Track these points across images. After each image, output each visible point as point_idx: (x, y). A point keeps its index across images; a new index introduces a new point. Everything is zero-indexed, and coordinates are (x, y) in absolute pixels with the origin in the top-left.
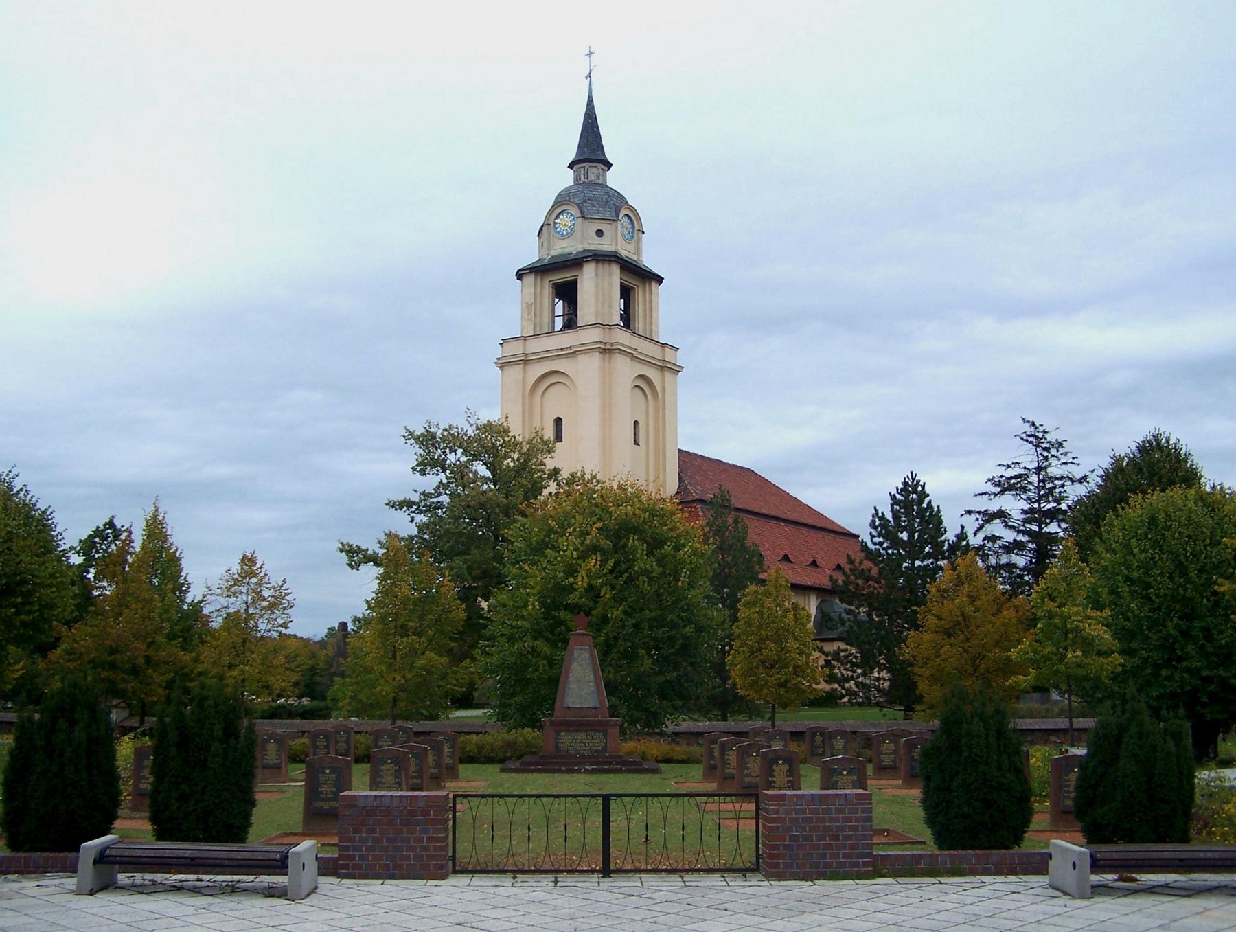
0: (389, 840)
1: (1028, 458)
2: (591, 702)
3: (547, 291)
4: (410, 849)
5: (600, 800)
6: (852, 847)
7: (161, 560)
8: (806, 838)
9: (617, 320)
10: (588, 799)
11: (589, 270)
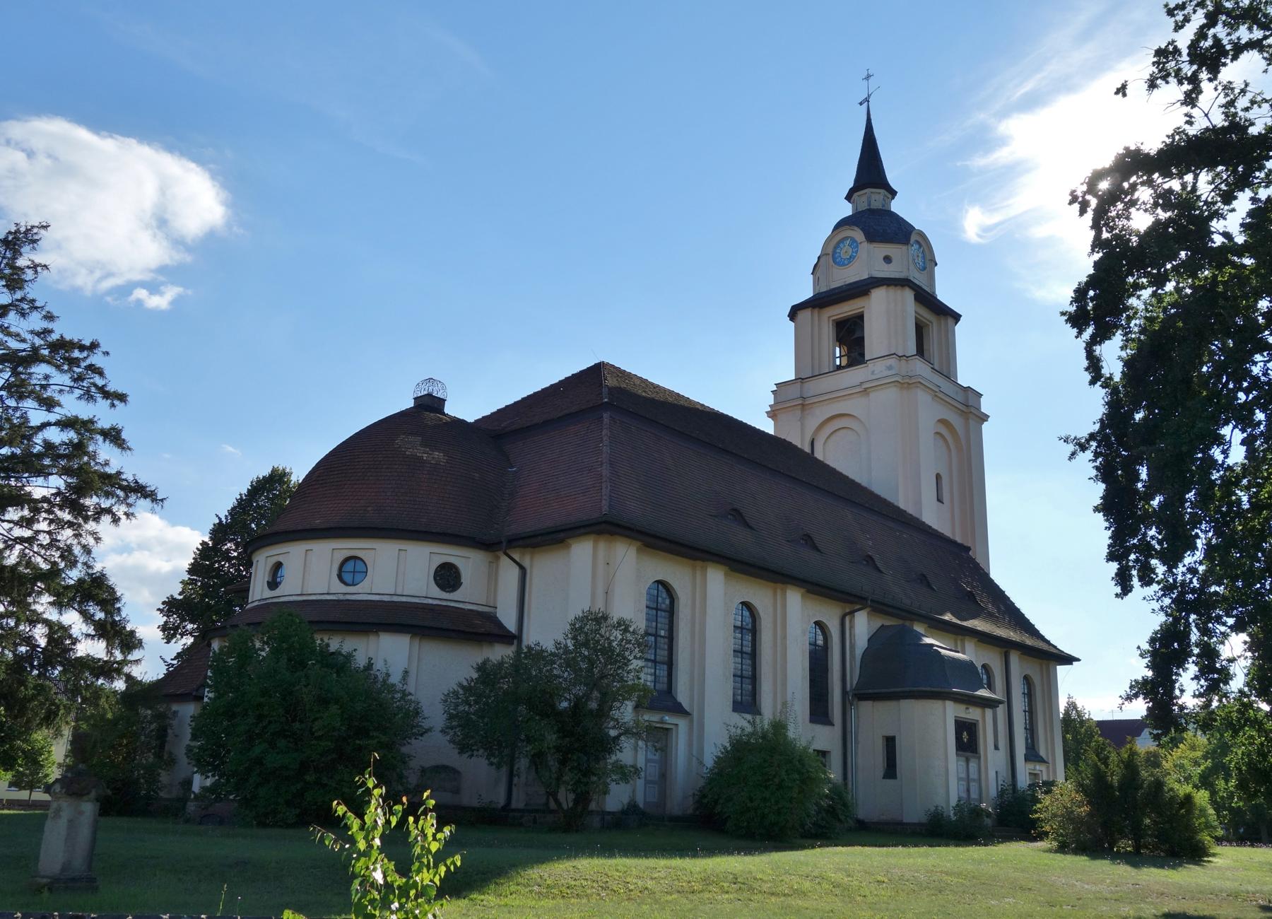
3: (828, 332)
7: (718, 757)
9: (912, 348)
11: (878, 295)
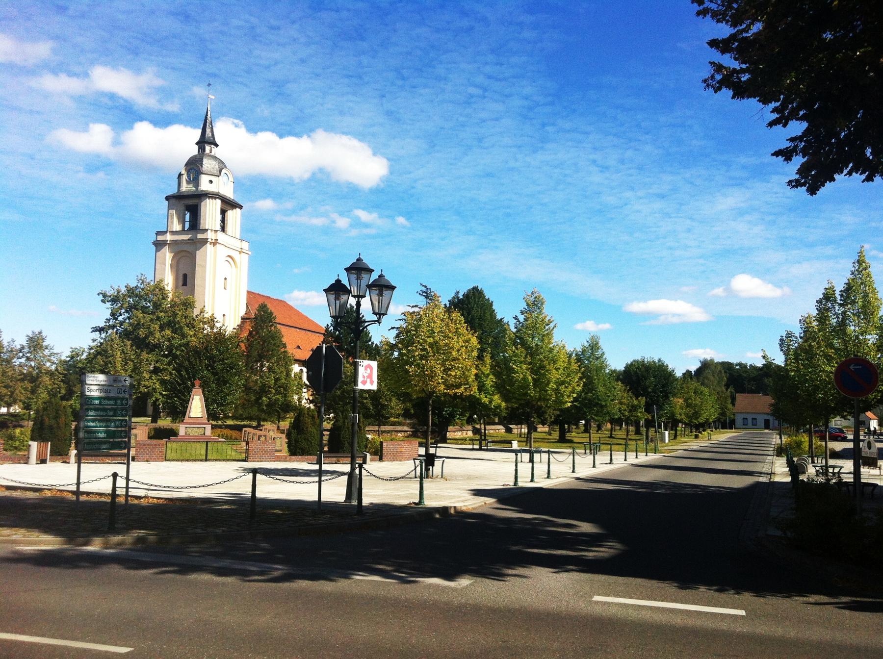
2: (199, 415)
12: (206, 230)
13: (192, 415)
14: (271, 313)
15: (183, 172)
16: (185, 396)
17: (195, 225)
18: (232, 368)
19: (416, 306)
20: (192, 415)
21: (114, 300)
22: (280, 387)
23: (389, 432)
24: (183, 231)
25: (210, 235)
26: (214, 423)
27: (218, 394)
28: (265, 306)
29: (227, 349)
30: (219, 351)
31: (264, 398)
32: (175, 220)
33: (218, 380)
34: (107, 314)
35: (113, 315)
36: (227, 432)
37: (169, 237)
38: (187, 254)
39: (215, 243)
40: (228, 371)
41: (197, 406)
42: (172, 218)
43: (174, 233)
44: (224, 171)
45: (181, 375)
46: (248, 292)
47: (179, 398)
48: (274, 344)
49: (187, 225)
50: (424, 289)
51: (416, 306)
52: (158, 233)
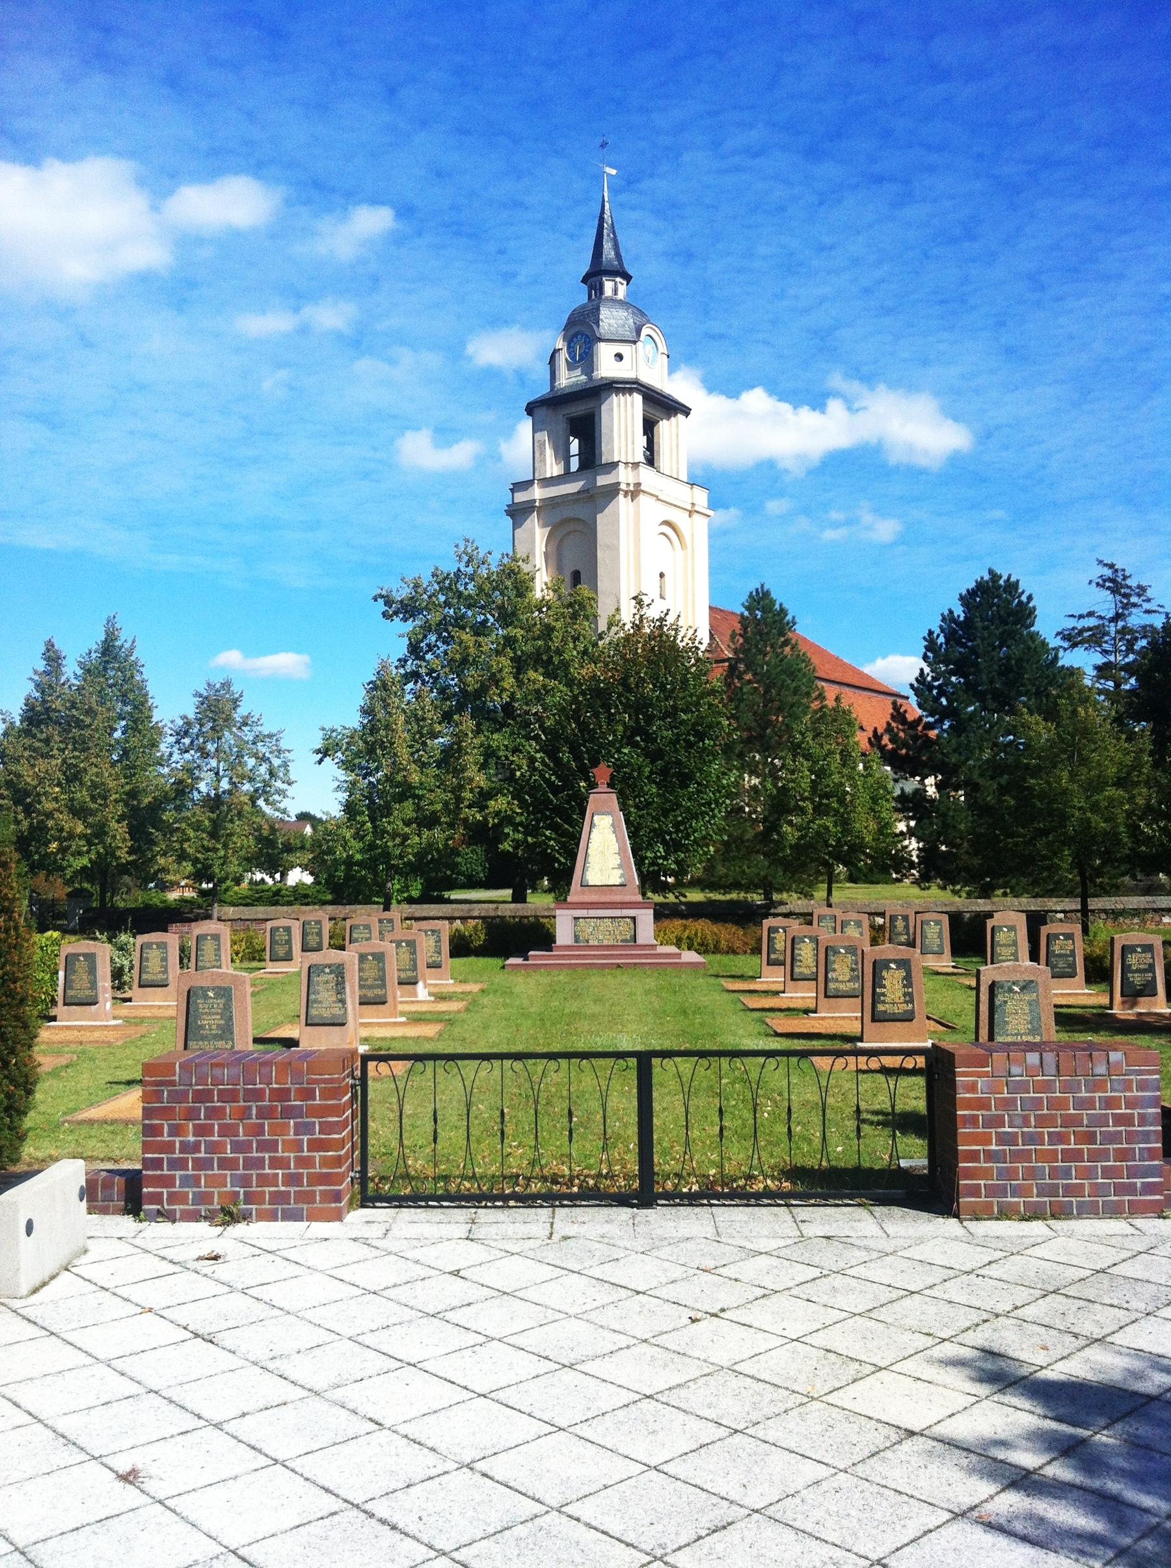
0: (238, 1147)
1: (1105, 603)
2: (615, 878)
4: (276, 1163)
5: (633, 1062)
6: (1122, 1155)
8: (1031, 1139)
10: (610, 1062)
12: (614, 465)
13: (594, 877)
14: (783, 611)
15: (560, 344)
16: (569, 820)
17: (591, 460)
18: (701, 737)
19: (1091, 614)
20: (594, 877)
21: (408, 609)
22: (827, 796)
23: (1136, 913)
24: (567, 476)
25: (624, 476)
26: (658, 898)
27: (666, 812)
28: (766, 594)
29: (685, 681)
30: (663, 688)
31: (786, 828)
32: (549, 452)
33: (664, 772)
34: (401, 648)
35: (414, 649)
36: (703, 927)
37: (538, 493)
38: (577, 521)
39: (635, 492)
40: (690, 745)
41: (605, 850)
42: (543, 453)
43: (547, 482)
44: (645, 331)
45: (558, 762)
46: (711, 608)
47: (554, 827)
48: (796, 691)
49: (575, 464)
50: (1108, 572)
51: (1091, 614)
52: (518, 487)
